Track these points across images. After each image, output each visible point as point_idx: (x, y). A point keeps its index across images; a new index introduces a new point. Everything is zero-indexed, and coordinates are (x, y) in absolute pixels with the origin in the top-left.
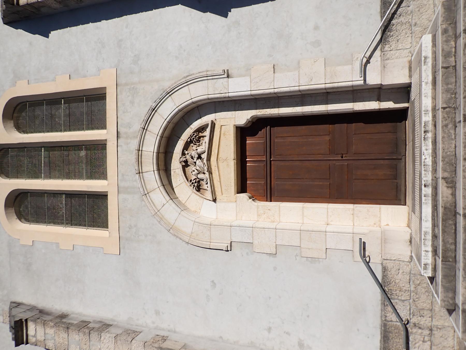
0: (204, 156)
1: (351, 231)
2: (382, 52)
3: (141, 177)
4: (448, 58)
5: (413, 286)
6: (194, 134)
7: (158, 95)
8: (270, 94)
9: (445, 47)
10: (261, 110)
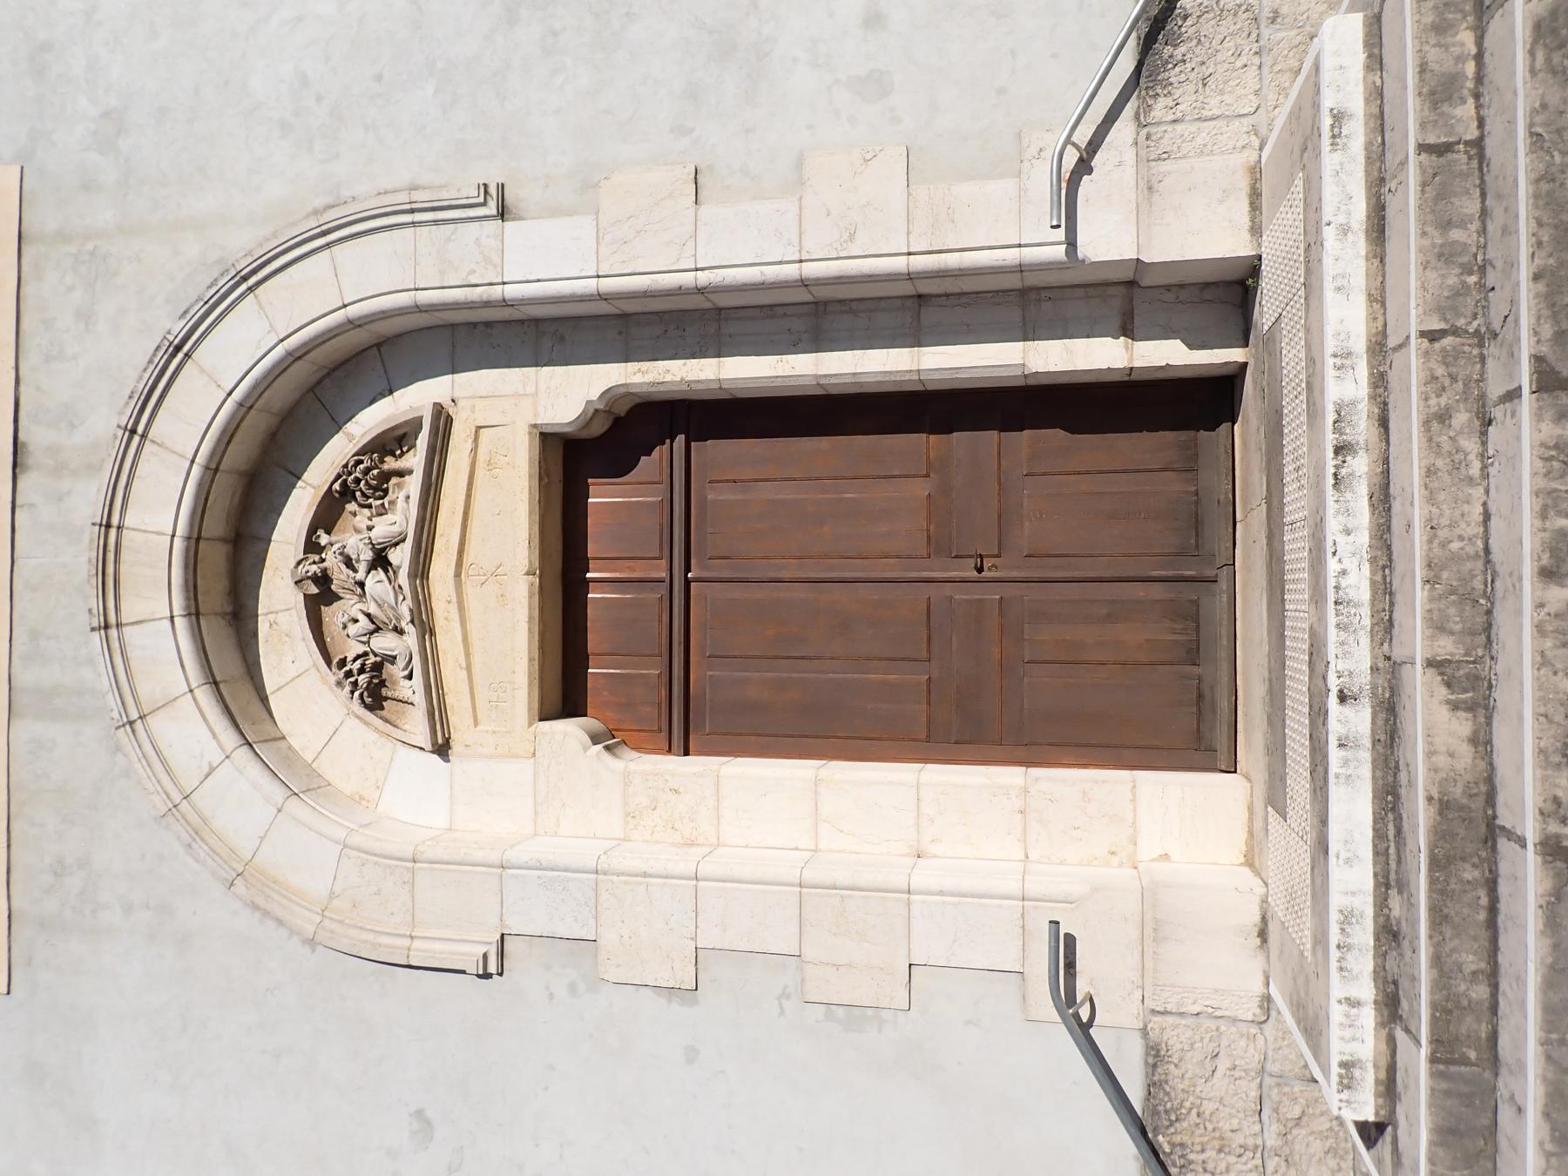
0: (401, 557)
1: (1014, 887)
2: (1141, 126)
3: (115, 645)
4: (1445, 108)
5: (1274, 1127)
6: (360, 462)
7: (199, 287)
8: (679, 292)
9: (1433, 54)
10: (645, 365)
